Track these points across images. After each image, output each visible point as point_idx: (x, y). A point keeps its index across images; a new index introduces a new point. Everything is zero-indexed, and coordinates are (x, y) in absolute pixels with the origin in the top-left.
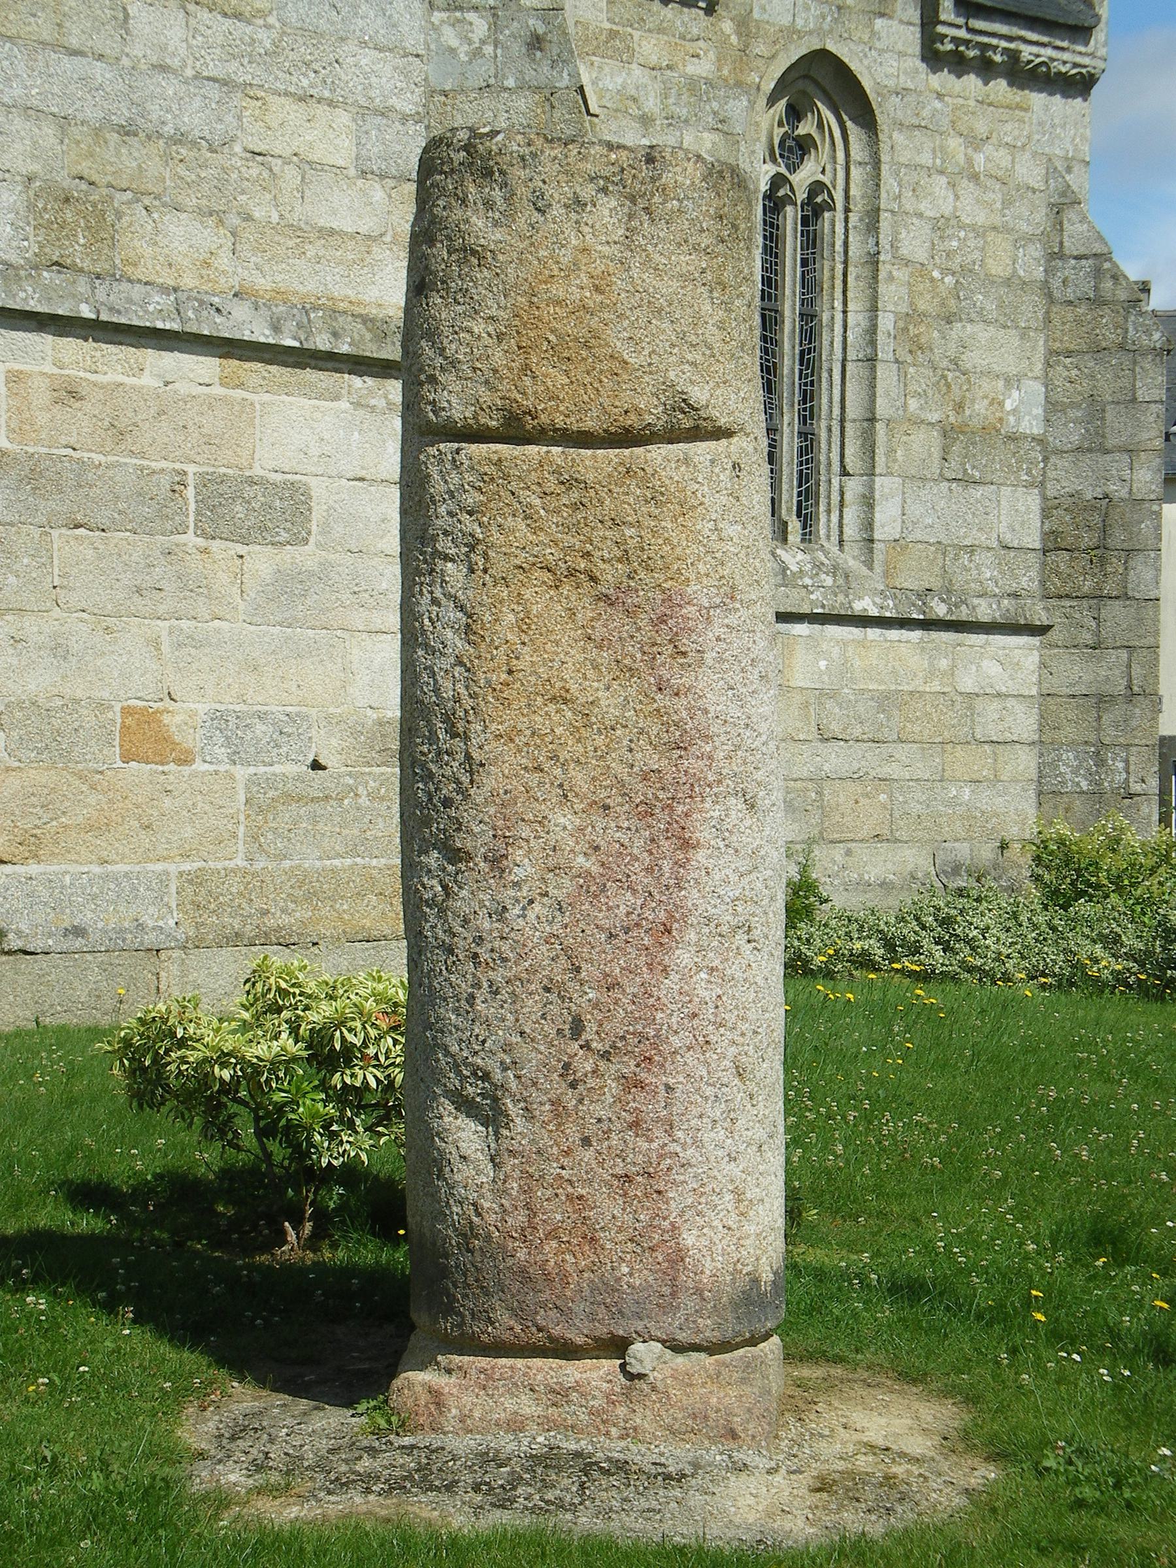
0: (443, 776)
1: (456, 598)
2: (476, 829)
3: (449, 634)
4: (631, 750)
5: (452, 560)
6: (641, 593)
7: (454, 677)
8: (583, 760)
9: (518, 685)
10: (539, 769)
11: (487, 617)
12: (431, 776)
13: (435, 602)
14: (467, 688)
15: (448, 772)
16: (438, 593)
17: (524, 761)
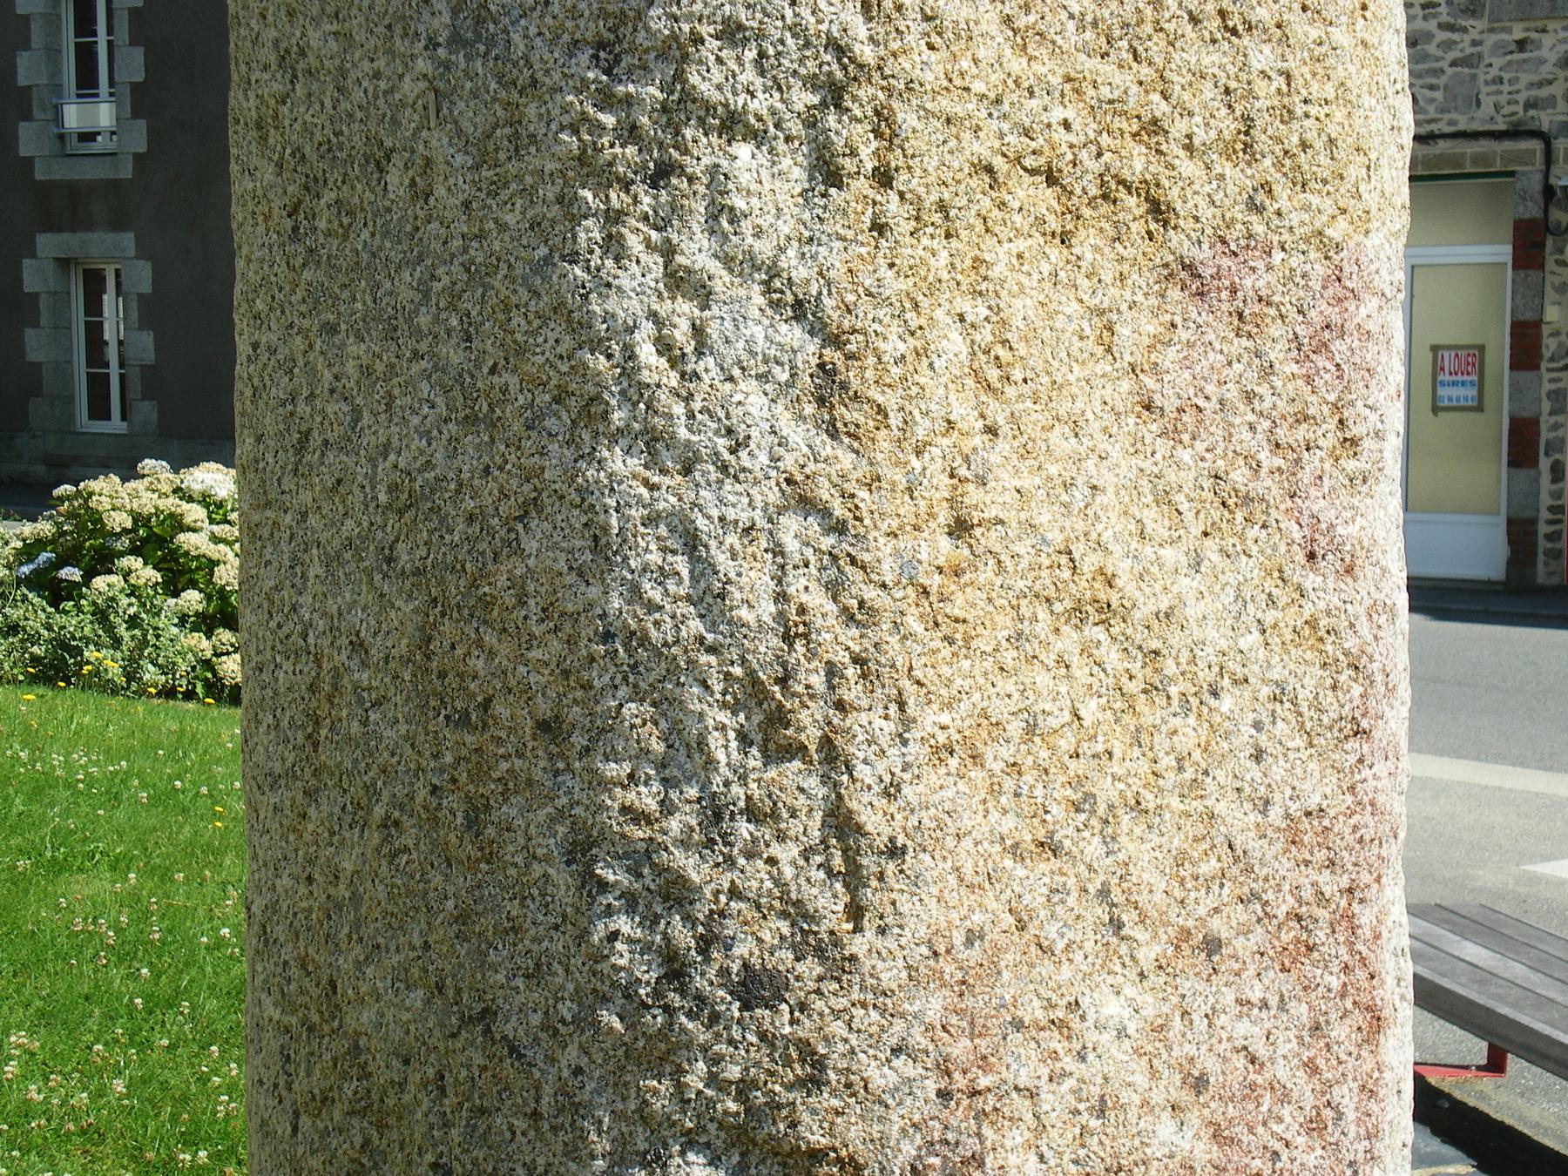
0: (735, 893)
1: (774, 272)
2: (880, 1077)
3: (753, 401)
4: (1258, 756)
5: (757, 137)
6: (1278, 256)
7: (777, 550)
8: (1149, 800)
9: (986, 574)
10: (1049, 847)
11: (893, 345)
12: (677, 893)
13: (679, 281)
14: (834, 589)
15: (756, 877)
16: (698, 252)
17: (1009, 823)
